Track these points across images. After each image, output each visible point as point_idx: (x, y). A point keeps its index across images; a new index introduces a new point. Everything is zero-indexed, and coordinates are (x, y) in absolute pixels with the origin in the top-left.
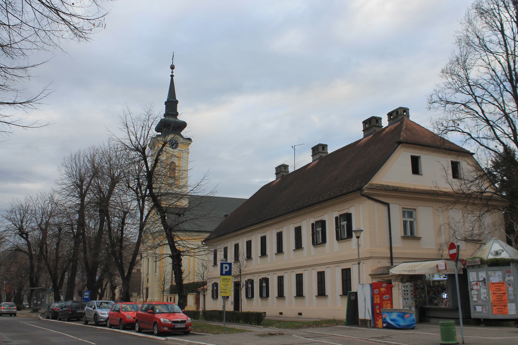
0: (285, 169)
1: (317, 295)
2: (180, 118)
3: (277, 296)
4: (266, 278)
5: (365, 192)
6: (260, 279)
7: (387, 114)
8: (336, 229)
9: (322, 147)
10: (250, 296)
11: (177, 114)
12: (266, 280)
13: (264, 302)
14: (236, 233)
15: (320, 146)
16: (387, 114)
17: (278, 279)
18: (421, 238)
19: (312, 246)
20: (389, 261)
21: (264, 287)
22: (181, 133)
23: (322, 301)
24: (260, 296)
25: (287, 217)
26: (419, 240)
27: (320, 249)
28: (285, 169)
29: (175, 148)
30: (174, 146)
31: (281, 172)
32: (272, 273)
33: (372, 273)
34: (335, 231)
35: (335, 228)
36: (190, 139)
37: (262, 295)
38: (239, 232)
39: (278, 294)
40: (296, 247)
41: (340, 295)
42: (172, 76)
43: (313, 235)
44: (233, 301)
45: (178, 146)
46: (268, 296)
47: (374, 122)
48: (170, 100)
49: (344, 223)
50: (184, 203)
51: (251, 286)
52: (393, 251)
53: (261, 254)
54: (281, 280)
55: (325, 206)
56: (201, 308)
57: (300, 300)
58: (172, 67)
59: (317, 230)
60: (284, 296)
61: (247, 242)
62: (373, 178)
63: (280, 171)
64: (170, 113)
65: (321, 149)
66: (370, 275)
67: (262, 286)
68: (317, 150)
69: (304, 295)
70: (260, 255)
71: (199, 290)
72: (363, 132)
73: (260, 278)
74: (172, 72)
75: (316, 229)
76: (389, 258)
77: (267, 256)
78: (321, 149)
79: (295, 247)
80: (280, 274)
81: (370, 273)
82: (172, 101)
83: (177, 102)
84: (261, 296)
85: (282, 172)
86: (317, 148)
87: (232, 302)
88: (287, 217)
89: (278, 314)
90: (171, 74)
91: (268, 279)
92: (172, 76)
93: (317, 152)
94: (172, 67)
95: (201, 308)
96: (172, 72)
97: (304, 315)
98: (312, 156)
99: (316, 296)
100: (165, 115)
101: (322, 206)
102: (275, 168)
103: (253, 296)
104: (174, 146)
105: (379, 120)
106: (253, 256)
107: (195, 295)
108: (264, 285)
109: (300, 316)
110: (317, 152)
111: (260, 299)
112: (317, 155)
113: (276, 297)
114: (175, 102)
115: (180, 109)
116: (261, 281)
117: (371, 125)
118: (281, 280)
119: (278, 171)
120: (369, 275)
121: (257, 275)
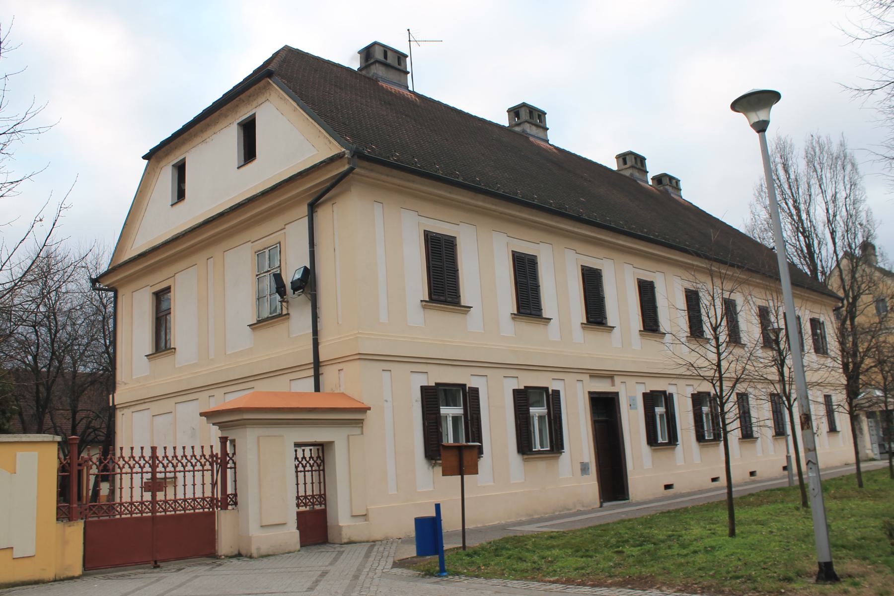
13: (663, 455)
37: (703, 436)
88: (754, 280)
103: (673, 439)
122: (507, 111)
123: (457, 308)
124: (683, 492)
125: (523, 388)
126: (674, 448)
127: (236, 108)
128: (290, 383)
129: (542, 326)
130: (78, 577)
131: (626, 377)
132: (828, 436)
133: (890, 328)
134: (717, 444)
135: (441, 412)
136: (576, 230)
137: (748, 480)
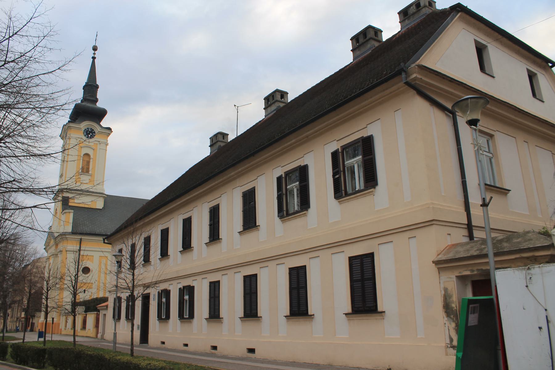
0: (223, 139)
1: (288, 314)
2: (99, 105)
3: (207, 316)
4: (189, 286)
5: (414, 76)
6: (180, 289)
7: (398, 13)
8: (334, 176)
9: (280, 94)
10: (164, 317)
11: (96, 100)
12: (190, 290)
13: (186, 326)
14: (147, 220)
15: (277, 93)
16: (398, 13)
17: (210, 286)
18: (509, 190)
19: (277, 219)
20: (465, 232)
21: (186, 301)
22: (101, 123)
23: (300, 325)
24: (158, 317)
25: (230, 175)
26: (506, 194)
27: (296, 223)
28: (223, 139)
29: (91, 138)
30: (90, 136)
31: (217, 142)
32: (199, 278)
33: (442, 257)
34: (332, 179)
35: (332, 174)
36: (109, 129)
37: (183, 315)
38: (152, 217)
39: (210, 314)
40: (244, 226)
41: (346, 314)
42: (94, 58)
43: (280, 198)
44: (140, 324)
45: (95, 136)
46: (192, 316)
47: (371, 34)
48: (89, 83)
49: (353, 160)
50: (100, 204)
51: (166, 301)
52: (472, 212)
53: (183, 247)
54: (215, 287)
55: (307, 137)
56: (100, 333)
57: (251, 324)
58: (95, 49)
59: (288, 187)
60: (221, 317)
61: (162, 231)
62: (442, 34)
63: (216, 141)
64: (88, 98)
65: (278, 97)
66: (436, 263)
67: (183, 299)
68: (273, 99)
69: (259, 315)
70: (182, 249)
71: (98, 308)
72: (352, 52)
73: (181, 286)
74: (94, 54)
75: (286, 186)
76: (466, 226)
77: (193, 250)
78: (279, 97)
79: (242, 227)
80: (214, 278)
81: (434, 258)
82: (90, 85)
83: (97, 87)
84: (181, 316)
85: (219, 142)
86: (273, 96)
87: (138, 325)
88: (230, 175)
89: (209, 350)
90: (93, 55)
91: (193, 287)
92: (94, 58)
93: (274, 101)
94: (95, 49)
95: (100, 333)
96: (94, 54)
97: (258, 354)
98: (264, 109)
99: (286, 316)
100: (82, 101)
101: (301, 137)
102: (210, 138)
103: (168, 317)
104: (90, 136)
105: (379, 33)
106: (171, 251)
107: (96, 315)
108: (187, 297)
109: (251, 355)
110: (274, 101)
111: (178, 322)
112: (273, 105)
113: (206, 319)
114: (95, 86)
115: (100, 94)
116: (182, 291)
117: (368, 38)
118: (215, 287)
119: (214, 142)
120: (433, 262)
121: (175, 282)
122: (351, 40)
123: (342, 199)
124: (169, 348)
125: (134, 294)
126: (167, 322)
127: (488, 35)
128: (409, 239)
129: (167, 260)
130: (94, 338)
131: (238, 268)
132: (288, 321)
133: (133, 234)
134: (190, 321)
135: (188, 296)
136: (191, 196)
137: (209, 352)
